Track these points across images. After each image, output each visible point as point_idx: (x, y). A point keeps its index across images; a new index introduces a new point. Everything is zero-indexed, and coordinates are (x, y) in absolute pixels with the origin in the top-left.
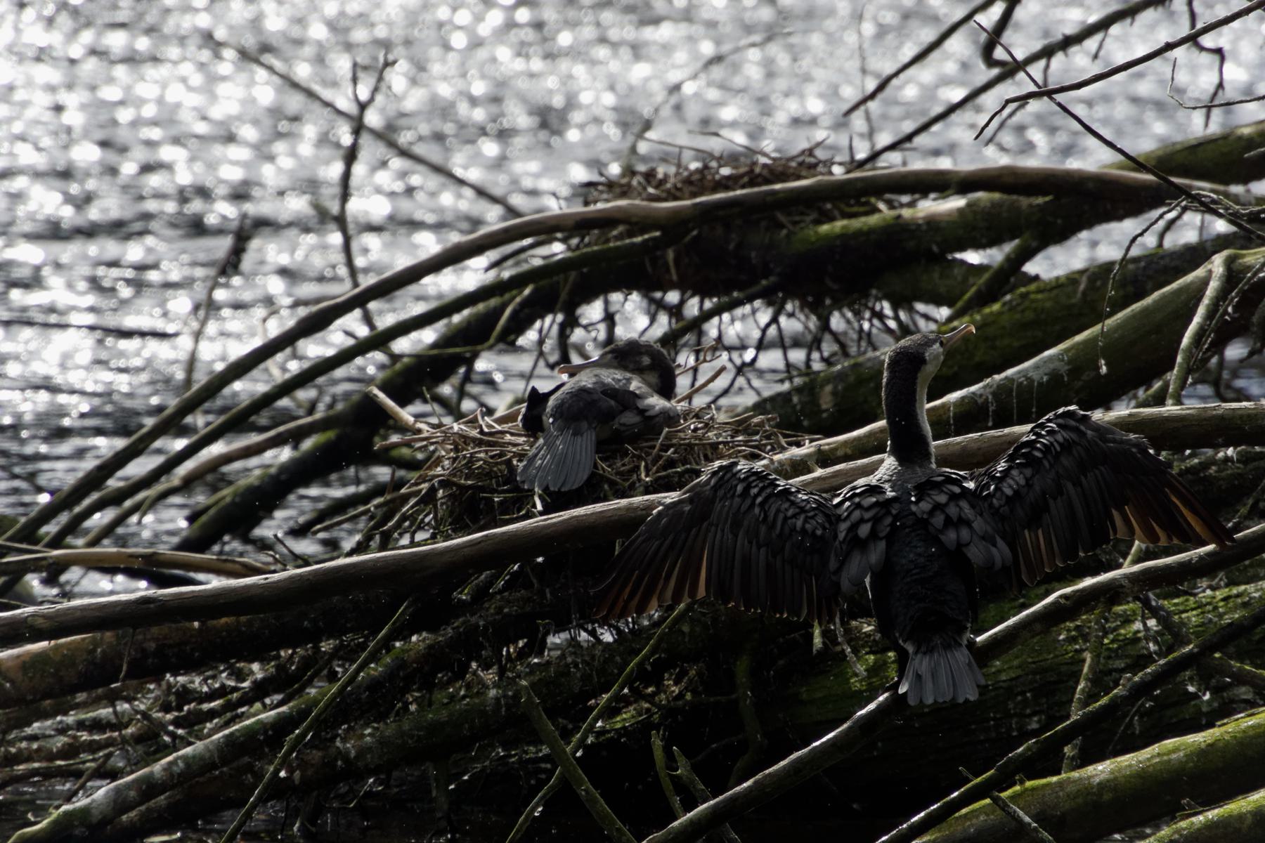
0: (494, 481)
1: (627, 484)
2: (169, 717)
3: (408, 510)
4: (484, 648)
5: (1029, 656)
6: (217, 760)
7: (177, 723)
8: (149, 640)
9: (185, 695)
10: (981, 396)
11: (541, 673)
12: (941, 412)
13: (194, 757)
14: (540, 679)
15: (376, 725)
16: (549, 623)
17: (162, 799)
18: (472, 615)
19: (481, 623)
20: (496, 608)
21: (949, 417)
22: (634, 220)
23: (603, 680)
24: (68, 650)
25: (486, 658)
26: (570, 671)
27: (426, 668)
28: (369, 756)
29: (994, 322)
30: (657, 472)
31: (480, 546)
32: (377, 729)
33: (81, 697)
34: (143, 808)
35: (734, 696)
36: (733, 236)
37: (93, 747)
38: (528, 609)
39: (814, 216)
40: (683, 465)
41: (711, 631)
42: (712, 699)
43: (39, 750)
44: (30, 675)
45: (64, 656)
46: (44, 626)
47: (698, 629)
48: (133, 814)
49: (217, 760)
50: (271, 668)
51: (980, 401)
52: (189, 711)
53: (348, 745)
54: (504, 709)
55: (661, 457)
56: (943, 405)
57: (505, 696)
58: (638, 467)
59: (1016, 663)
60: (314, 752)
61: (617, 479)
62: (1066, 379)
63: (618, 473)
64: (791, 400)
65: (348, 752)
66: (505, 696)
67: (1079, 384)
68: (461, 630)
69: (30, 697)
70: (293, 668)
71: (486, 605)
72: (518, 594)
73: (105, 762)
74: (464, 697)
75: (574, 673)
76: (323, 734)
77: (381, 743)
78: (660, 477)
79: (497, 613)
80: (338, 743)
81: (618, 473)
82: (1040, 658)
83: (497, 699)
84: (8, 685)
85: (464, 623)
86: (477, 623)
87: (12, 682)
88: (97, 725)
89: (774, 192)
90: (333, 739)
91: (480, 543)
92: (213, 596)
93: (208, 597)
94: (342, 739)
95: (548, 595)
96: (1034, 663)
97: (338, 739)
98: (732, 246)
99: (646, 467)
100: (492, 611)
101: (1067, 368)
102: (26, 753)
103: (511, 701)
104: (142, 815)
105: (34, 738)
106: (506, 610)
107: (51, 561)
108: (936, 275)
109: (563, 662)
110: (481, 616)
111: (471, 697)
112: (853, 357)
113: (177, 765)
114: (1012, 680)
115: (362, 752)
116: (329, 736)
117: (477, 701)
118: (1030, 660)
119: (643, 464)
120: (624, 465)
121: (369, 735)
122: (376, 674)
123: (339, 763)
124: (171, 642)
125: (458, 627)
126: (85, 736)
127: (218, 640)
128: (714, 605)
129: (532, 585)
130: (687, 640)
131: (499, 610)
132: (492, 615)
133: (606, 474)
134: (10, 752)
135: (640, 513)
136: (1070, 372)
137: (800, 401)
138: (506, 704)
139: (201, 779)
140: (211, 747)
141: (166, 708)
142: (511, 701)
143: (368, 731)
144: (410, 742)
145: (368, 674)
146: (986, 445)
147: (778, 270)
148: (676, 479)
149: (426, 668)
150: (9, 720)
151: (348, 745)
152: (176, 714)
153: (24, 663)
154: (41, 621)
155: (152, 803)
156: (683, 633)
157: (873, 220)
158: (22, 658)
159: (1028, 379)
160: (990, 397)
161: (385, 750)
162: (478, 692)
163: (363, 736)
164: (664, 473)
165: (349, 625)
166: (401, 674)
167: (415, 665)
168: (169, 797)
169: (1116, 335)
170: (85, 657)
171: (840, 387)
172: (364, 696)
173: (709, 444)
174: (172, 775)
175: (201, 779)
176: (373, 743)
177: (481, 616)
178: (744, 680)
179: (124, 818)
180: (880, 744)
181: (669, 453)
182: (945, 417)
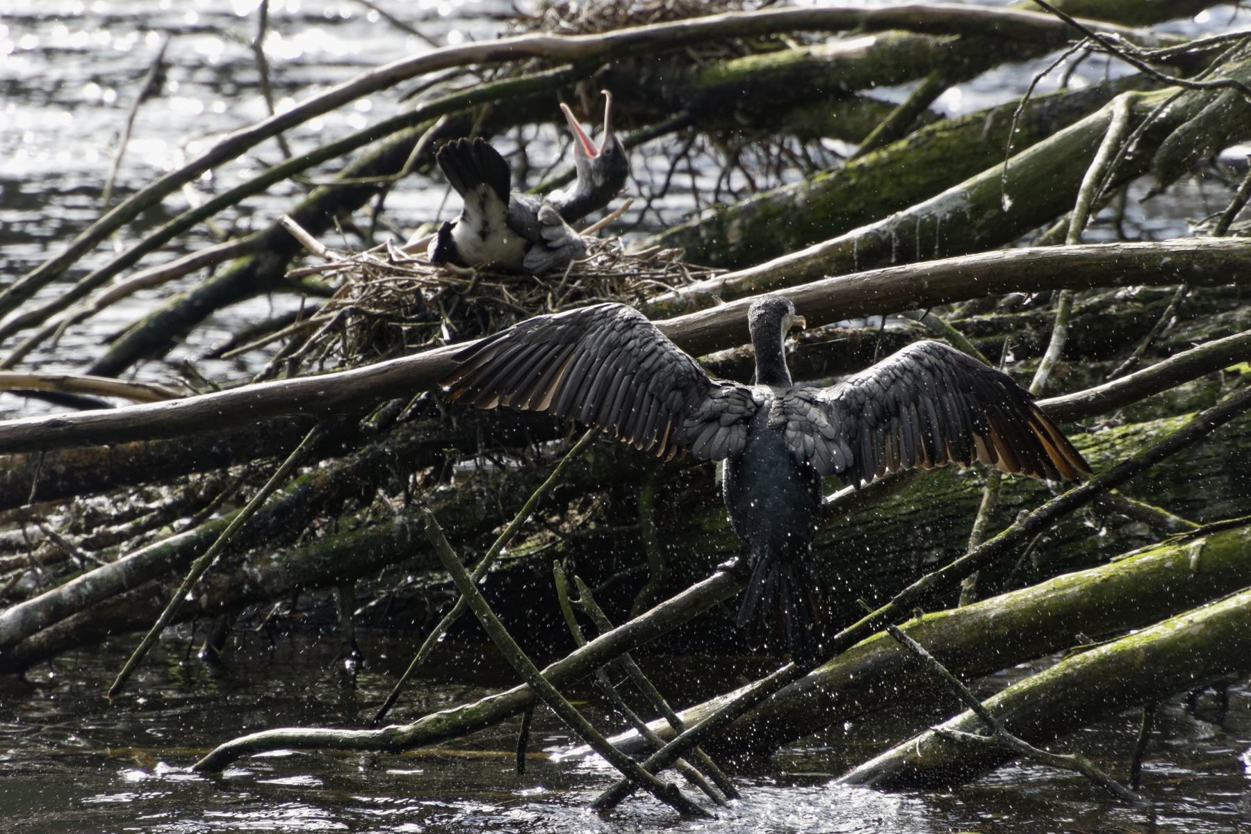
4: (391, 475)
8: (59, 463)
9: (95, 518)
10: (884, 232)
11: (447, 500)
13: (102, 579)
15: (282, 550)
16: (454, 452)
17: (70, 620)
18: (379, 442)
22: (546, 53)
25: (392, 486)
26: (475, 500)
27: (333, 494)
28: (275, 581)
32: (284, 554)
34: (51, 629)
39: (723, 52)
40: (590, 297)
48: (40, 635)
51: (884, 237)
52: (98, 533)
54: (409, 536)
57: (411, 523)
58: (545, 299)
60: (221, 576)
62: (968, 217)
65: (255, 577)
66: (411, 523)
67: (980, 222)
68: (368, 457)
71: (393, 433)
80: (245, 568)
83: (403, 526)
85: (371, 450)
91: (386, 371)
92: (122, 419)
94: (248, 563)
97: (245, 563)
98: (643, 80)
100: (399, 439)
101: (969, 206)
104: (50, 635)
106: (413, 438)
108: (844, 112)
111: (377, 524)
114: (912, 513)
115: (268, 577)
116: (236, 560)
117: (383, 527)
119: (550, 295)
120: (531, 296)
121: (276, 559)
123: (246, 587)
124: (80, 465)
125: (365, 454)
130: (591, 469)
131: (406, 438)
133: (514, 305)
136: (973, 210)
138: (412, 531)
139: (109, 601)
142: (416, 528)
143: (275, 556)
144: (316, 567)
147: (688, 104)
155: (60, 624)
156: (587, 463)
160: (894, 234)
162: (384, 519)
163: (270, 560)
166: (308, 499)
167: (322, 491)
168: (77, 618)
169: (1019, 174)
174: (80, 597)
175: (109, 601)
176: (279, 567)
177: (388, 444)
179: (32, 638)
181: (576, 284)
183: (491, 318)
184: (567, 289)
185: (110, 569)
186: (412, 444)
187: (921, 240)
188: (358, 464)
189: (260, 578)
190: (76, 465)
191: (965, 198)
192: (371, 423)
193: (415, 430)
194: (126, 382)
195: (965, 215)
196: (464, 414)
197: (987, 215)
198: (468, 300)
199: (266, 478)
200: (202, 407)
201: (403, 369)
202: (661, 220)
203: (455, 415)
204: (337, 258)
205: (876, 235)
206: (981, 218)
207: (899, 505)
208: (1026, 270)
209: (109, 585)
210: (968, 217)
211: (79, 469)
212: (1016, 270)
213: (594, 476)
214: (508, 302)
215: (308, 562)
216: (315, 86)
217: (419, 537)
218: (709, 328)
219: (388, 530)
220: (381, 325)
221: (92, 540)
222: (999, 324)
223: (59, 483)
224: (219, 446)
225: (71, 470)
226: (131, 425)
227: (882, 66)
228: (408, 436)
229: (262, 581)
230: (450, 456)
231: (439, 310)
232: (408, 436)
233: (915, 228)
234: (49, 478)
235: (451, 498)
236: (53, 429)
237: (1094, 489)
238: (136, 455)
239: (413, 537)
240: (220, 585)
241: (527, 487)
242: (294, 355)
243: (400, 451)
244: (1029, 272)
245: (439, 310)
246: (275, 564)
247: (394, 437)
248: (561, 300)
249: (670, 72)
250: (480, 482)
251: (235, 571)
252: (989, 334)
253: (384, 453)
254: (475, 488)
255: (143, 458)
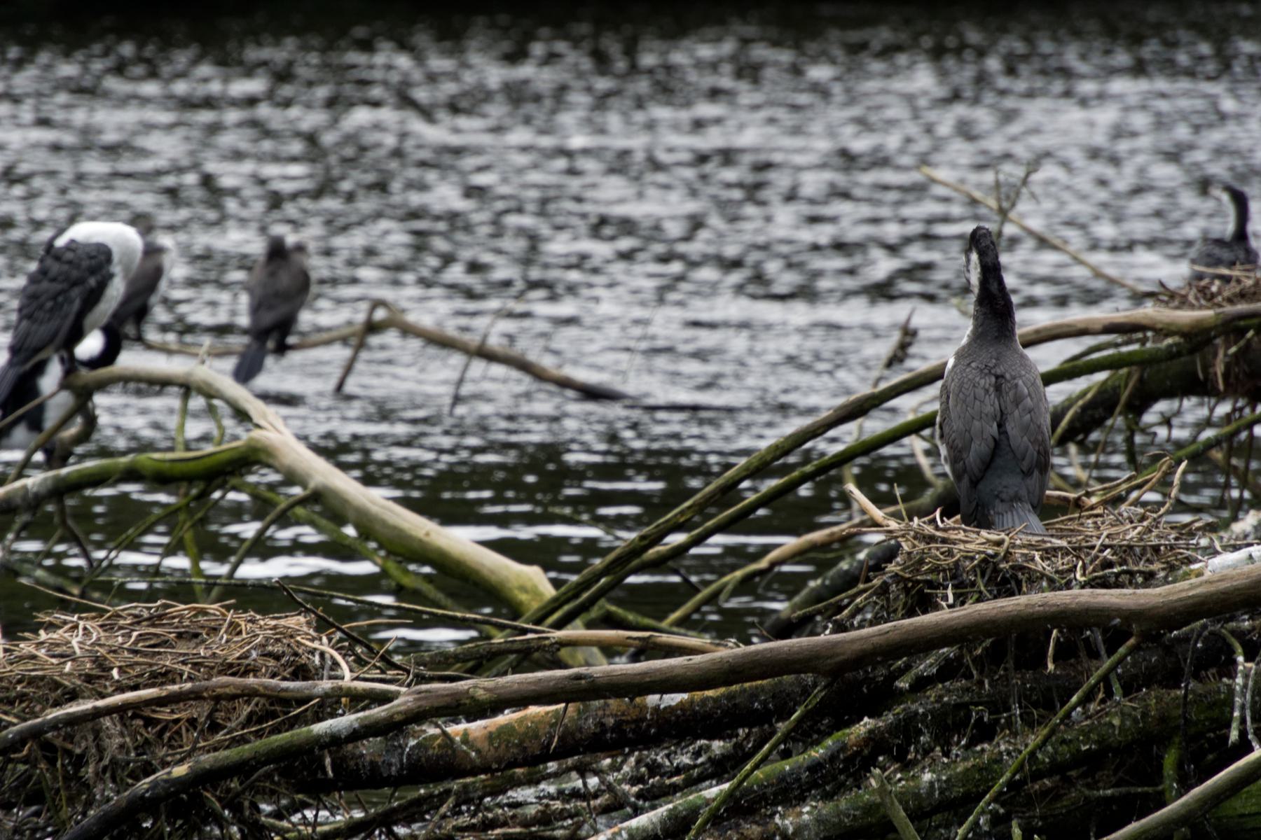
0: (941, 575)
1: (1063, 581)
2: (635, 789)
7: (639, 795)
11: (975, 759)
14: (973, 766)
15: (814, 804)
18: (912, 703)
19: (921, 711)
23: (1034, 768)
24: (532, 722)
25: (924, 744)
26: (1002, 759)
27: (866, 752)
28: (806, 833)
30: (1094, 571)
31: (887, 635)
33: (552, 766)
35: (1160, 788)
37: (563, 815)
38: (966, 699)
41: (1141, 725)
42: (282, 765)
43: (514, 817)
44: (496, 745)
45: (528, 728)
47: (1128, 723)
54: (937, 792)
57: (939, 780)
58: (1075, 567)
60: (754, 827)
61: (1056, 577)
63: (1057, 572)
65: (786, 829)
66: (939, 780)
68: (901, 716)
69: (495, 766)
71: (928, 693)
72: (959, 684)
73: (574, 833)
75: (1007, 761)
78: (1096, 577)
80: (777, 819)
81: (1057, 572)
83: (931, 783)
85: (904, 710)
86: (917, 710)
87: (478, 751)
88: (575, 794)
92: (639, 674)
93: (635, 675)
94: (781, 815)
95: (987, 686)
97: (778, 816)
99: (1084, 568)
100: (932, 699)
102: (502, 818)
103: (944, 785)
106: (946, 699)
107: (553, 641)
109: (996, 751)
111: (907, 780)
112: (317, 214)
113: (621, 835)
115: (799, 830)
116: (769, 813)
117: (912, 784)
119: (1080, 563)
121: (807, 813)
122: (817, 755)
124: (629, 718)
125: (898, 714)
126: (557, 805)
127: (673, 718)
129: (972, 676)
130: (1117, 732)
131: (940, 698)
132: (932, 703)
133: (1047, 573)
135: (1037, 609)
138: (940, 788)
140: (654, 820)
141: (634, 781)
142: (944, 785)
143: (807, 809)
144: (846, 820)
149: (866, 752)
150: (485, 787)
152: (641, 786)
153: (491, 733)
154: (481, 692)
156: (1113, 726)
158: (489, 729)
162: (913, 776)
163: (801, 813)
164: (1101, 573)
167: (855, 748)
170: (547, 730)
178: (1171, 772)
183: (1024, 584)
184: (1097, 557)
186: (944, 705)
188: (891, 723)
189: (791, 830)
190: (624, 718)
192: (903, 684)
193: (949, 691)
194: (502, 640)
196: (997, 677)
198: (1002, 566)
199: (264, 776)
201: (904, 630)
202: (245, 332)
209: (645, 834)
211: (627, 722)
213: (1120, 739)
215: (838, 815)
216: (94, 154)
217: (947, 794)
220: (921, 590)
221: (648, 790)
223: (609, 735)
224: (760, 703)
225: (618, 726)
226: (648, 679)
228: (941, 697)
229: (793, 834)
232: (941, 697)
234: (598, 730)
235: (980, 757)
236: (575, 682)
238: (681, 709)
239: (940, 793)
241: (1053, 748)
242: (838, 617)
243: (932, 712)
245: (976, 576)
246: (806, 817)
247: (928, 698)
248: (1091, 568)
253: (916, 713)
254: (1003, 748)
255: (688, 713)
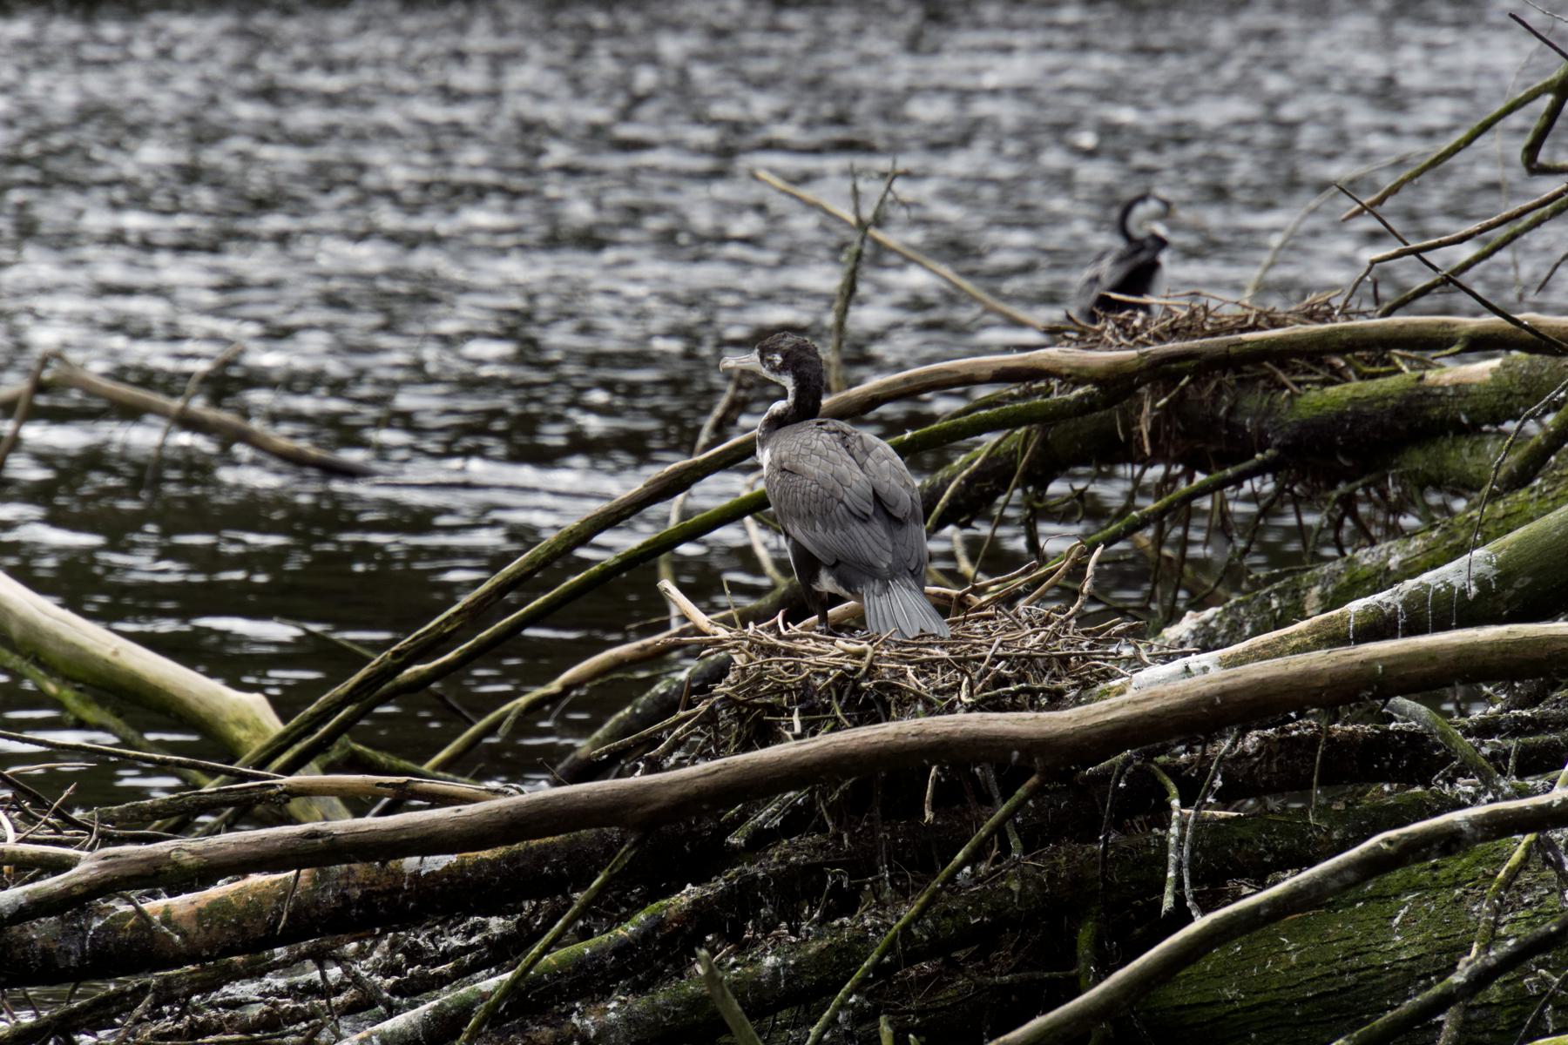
3: (682, 733)
4: (763, 905)
5: (1435, 931)
6: (421, 1037)
7: (394, 990)
8: (353, 886)
9: (414, 955)
10: (1388, 605)
12: (1339, 623)
13: (392, 1033)
14: (830, 945)
16: (840, 873)
18: (750, 864)
20: (780, 855)
21: (1348, 631)
22: (1066, 371)
24: (254, 896)
25: (765, 918)
29: (1519, 512)
30: (984, 690)
33: (280, 953)
36: (1225, 398)
39: (1323, 374)
40: (1019, 683)
43: (231, 1019)
45: (248, 902)
46: (191, 862)
49: (421, 1037)
50: (511, 923)
51: (1387, 611)
52: (412, 976)
53: (587, 1022)
55: (989, 672)
56: (1342, 616)
57: (785, 966)
58: (960, 684)
59: (1419, 938)
60: (545, 1029)
61: (935, 698)
62: (1494, 586)
64: (1269, 604)
67: (1509, 593)
70: (538, 923)
71: (770, 852)
74: (734, 966)
76: (556, 1007)
77: (628, 1020)
79: (781, 862)
80: (575, 1019)
82: (1449, 934)
83: (775, 969)
84: (177, 937)
85: (739, 873)
86: (756, 874)
87: (183, 934)
88: (311, 989)
89: (1241, 343)
90: (568, 1015)
91: (716, 772)
96: (1441, 939)
97: (575, 1014)
98: (1222, 412)
100: (775, 859)
101: (1495, 572)
105: (229, 1005)
106: (793, 859)
108: (1465, 451)
110: (761, 866)
111: (744, 966)
114: (1414, 959)
115: (603, 1032)
117: (750, 971)
118: (1436, 935)
120: (943, 681)
121: (614, 1010)
124: (380, 888)
125: (731, 879)
126: (288, 1004)
128: (1053, 858)
131: (784, 858)
133: (923, 693)
134: (196, 1021)
136: (1499, 578)
137: (1280, 606)
138: (786, 975)
143: (613, 1005)
144: (665, 1019)
145: (616, 935)
146: (1334, 665)
147: (1277, 441)
148: (1009, 700)
151: (587, 1022)
154: (187, 856)
156: (1011, 892)
157: (1390, 382)
159: (1447, 585)
160: (1400, 607)
161: (633, 1029)
162: (751, 960)
165: (967, 870)
166: (658, 935)
169: (1558, 533)
171: (1329, 590)
172: (609, 962)
173: (1056, 656)
176: (618, 1020)
177: (761, 866)
178: (1087, 952)
180: (1253, 1036)
181: (998, 667)
182: (1342, 630)
183: (893, 708)
185: (404, 1020)
186: (791, 866)
187: (1433, 615)
191: (1490, 563)
195: (1490, 583)
197: (1517, 585)
198: (864, 684)
200: (490, 815)
201: (737, 769)
203: (846, 830)
204: (722, 633)
205: (1378, 609)
206: (1510, 588)
207: (1399, 948)
208: (1503, 653)
210: (1494, 586)
211: (378, 893)
212: (1492, 653)
213: (1019, 909)
214: (914, 688)
215: (654, 1013)
218: (1113, 721)
219: (755, 974)
222: (1542, 720)
226: (404, 837)
227: (1510, 394)
230: (833, 878)
231: (830, 698)
232: (787, 856)
233: (1427, 600)
236: (310, 841)
237: (1557, 932)
240: (543, 1042)
241: (934, 922)
244: (1508, 655)
245: (830, 698)
246: (612, 1015)
248: (980, 685)
249: (1253, 401)
250: (876, 914)
251: (563, 1023)
252: (1530, 734)
